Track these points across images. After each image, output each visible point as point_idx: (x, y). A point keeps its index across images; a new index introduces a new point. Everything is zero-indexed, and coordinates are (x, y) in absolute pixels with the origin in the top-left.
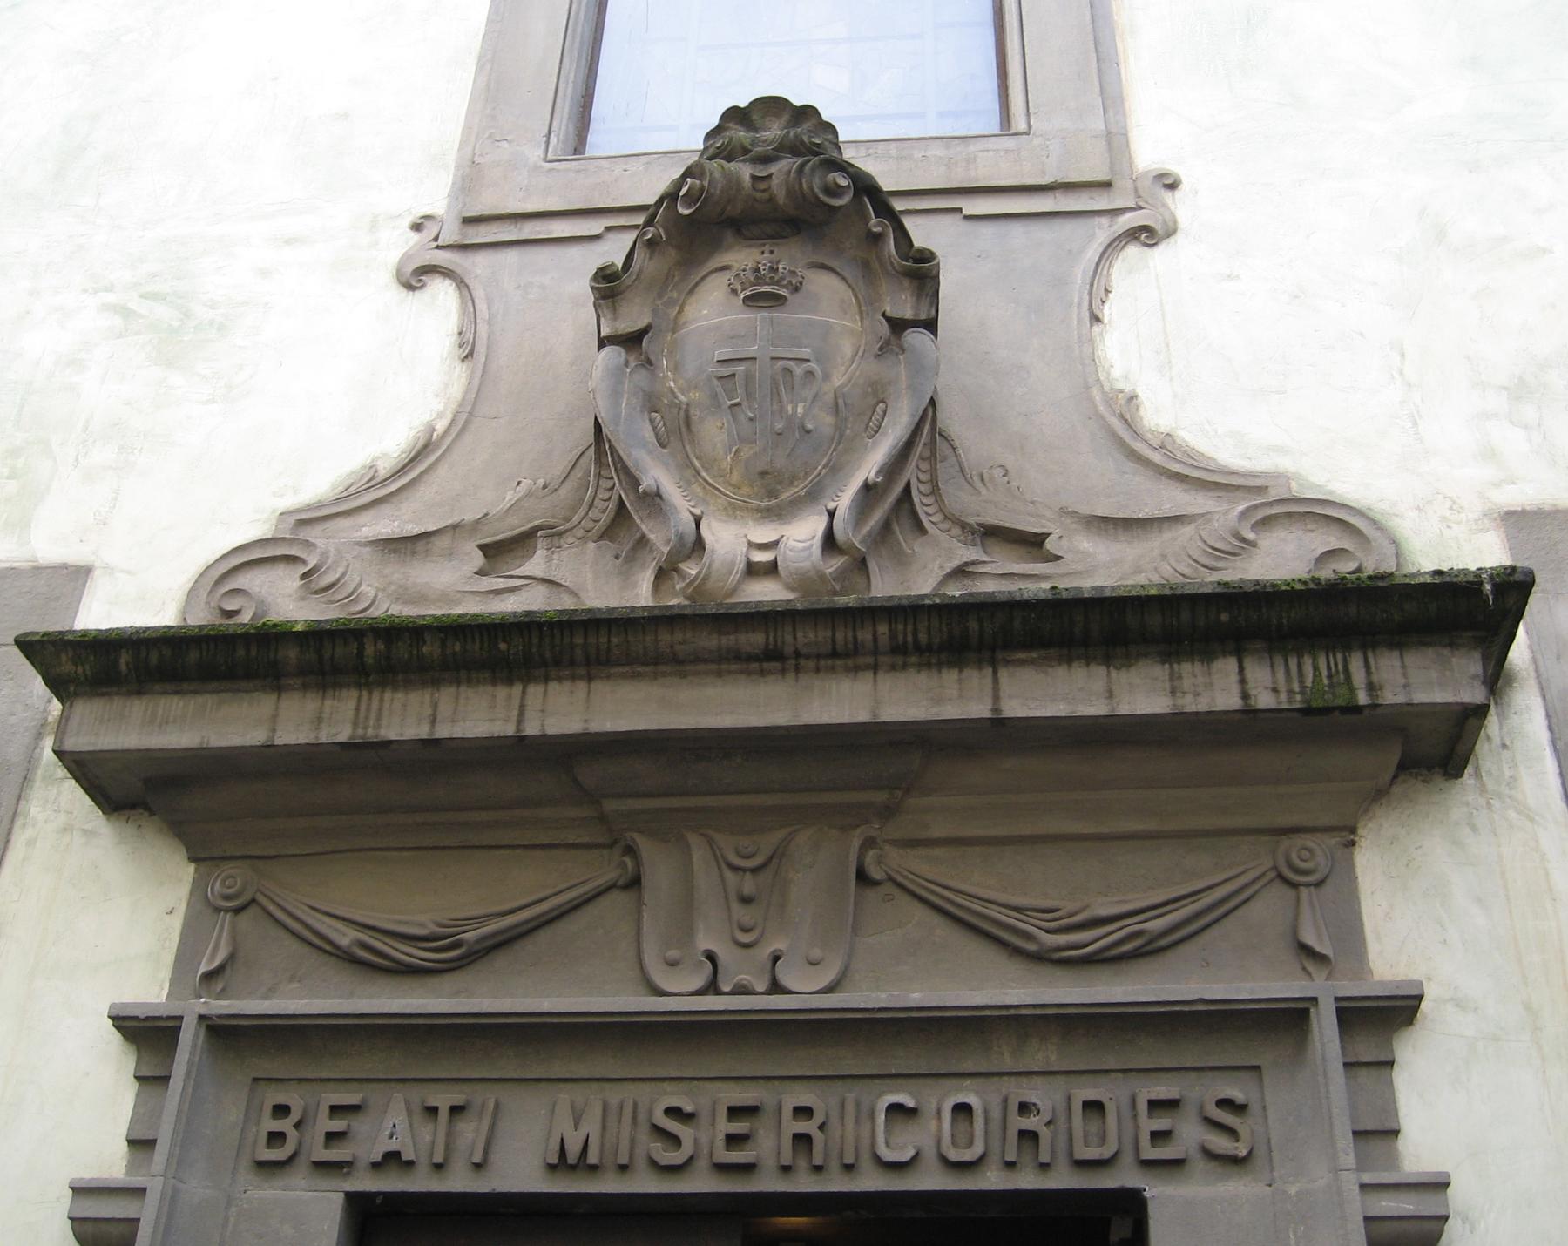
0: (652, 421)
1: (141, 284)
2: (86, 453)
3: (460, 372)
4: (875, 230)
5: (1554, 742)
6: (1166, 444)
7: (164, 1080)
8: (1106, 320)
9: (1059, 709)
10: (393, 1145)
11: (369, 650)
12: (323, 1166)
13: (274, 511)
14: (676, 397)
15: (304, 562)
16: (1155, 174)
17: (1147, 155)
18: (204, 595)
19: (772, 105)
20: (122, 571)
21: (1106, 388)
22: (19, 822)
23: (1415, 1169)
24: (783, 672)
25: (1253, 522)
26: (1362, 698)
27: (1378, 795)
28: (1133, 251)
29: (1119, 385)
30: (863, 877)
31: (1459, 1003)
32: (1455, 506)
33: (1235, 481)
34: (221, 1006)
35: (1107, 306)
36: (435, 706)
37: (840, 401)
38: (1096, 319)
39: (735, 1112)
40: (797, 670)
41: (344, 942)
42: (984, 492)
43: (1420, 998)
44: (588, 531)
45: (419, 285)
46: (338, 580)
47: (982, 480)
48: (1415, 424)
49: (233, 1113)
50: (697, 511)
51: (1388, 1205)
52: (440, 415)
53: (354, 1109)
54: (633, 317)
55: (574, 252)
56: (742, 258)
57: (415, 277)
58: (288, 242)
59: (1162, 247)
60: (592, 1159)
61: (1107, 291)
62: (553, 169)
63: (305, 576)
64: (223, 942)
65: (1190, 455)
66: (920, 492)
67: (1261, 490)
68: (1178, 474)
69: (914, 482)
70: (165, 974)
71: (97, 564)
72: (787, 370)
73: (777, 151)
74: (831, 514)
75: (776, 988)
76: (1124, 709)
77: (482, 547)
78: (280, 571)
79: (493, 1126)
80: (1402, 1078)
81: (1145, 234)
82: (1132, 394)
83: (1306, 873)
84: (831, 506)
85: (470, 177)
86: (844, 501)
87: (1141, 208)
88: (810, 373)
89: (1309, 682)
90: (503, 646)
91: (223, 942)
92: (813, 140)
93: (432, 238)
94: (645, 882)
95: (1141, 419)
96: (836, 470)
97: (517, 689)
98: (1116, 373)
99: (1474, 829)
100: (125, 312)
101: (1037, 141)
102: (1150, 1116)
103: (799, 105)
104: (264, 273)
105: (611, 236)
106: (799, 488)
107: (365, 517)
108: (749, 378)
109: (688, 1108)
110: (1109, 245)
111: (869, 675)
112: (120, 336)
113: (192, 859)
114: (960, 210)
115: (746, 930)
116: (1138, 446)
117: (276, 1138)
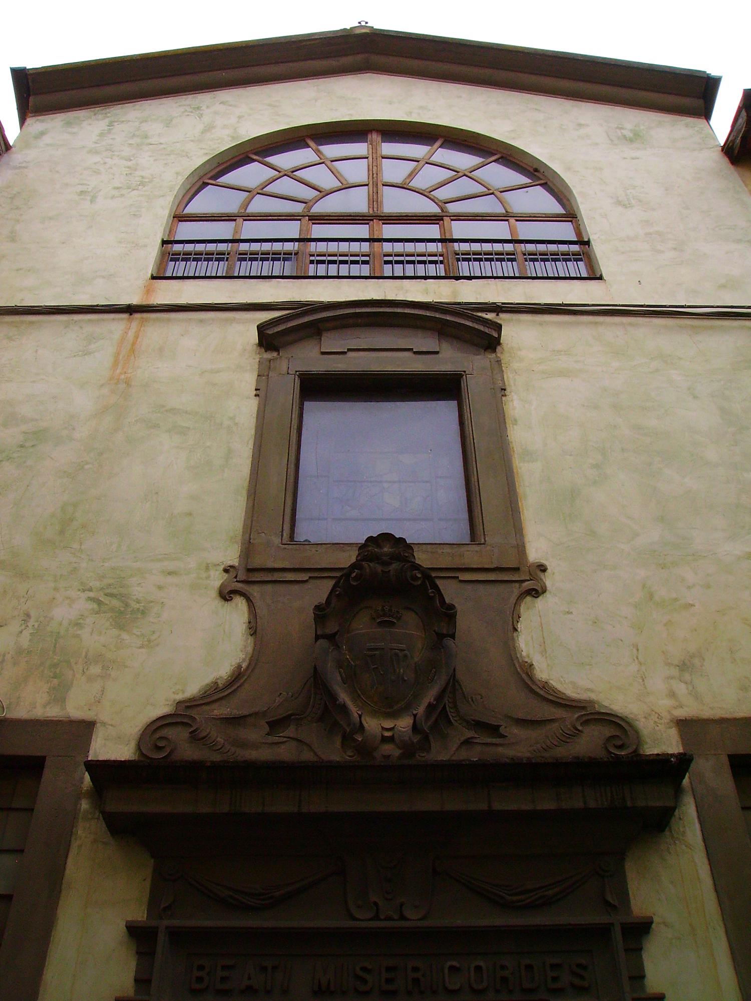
0: (340, 672)
1: (104, 589)
2: (87, 669)
3: (251, 640)
4: (430, 595)
5: (699, 817)
6: (545, 685)
7: (153, 953)
8: (519, 630)
9: (514, 807)
13: (174, 701)
14: (350, 663)
15: (191, 726)
17: (534, 554)
19: (387, 537)
20: (109, 725)
21: (520, 661)
25: (581, 721)
26: (629, 804)
28: (528, 599)
31: (666, 924)
32: (660, 717)
33: (574, 704)
35: (519, 624)
37: (417, 667)
38: (515, 630)
39: (389, 969)
42: (473, 706)
43: (652, 923)
44: (313, 718)
45: (230, 599)
47: (472, 700)
48: (643, 680)
50: (360, 713)
52: (244, 660)
54: (332, 627)
57: (226, 595)
58: (170, 573)
59: (541, 598)
62: (285, 548)
63: (191, 733)
65: (555, 691)
66: (450, 707)
67: (584, 708)
68: (551, 700)
70: (144, 908)
71: (97, 721)
72: (397, 655)
73: (391, 559)
75: (403, 918)
76: (539, 808)
77: (266, 722)
78: (179, 729)
81: (534, 592)
82: (531, 664)
84: (415, 712)
85: (248, 549)
86: (421, 710)
88: (405, 656)
92: (405, 554)
93: (234, 577)
95: (535, 675)
98: (524, 654)
99: (670, 853)
100: (99, 603)
101: (489, 548)
103: (398, 537)
104: (160, 588)
105: (312, 581)
107: (215, 706)
109: (369, 967)
110: (518, 598)
113: (153, 857)
114: (458, 577)
116: (534, 687)
117: (200, 979)
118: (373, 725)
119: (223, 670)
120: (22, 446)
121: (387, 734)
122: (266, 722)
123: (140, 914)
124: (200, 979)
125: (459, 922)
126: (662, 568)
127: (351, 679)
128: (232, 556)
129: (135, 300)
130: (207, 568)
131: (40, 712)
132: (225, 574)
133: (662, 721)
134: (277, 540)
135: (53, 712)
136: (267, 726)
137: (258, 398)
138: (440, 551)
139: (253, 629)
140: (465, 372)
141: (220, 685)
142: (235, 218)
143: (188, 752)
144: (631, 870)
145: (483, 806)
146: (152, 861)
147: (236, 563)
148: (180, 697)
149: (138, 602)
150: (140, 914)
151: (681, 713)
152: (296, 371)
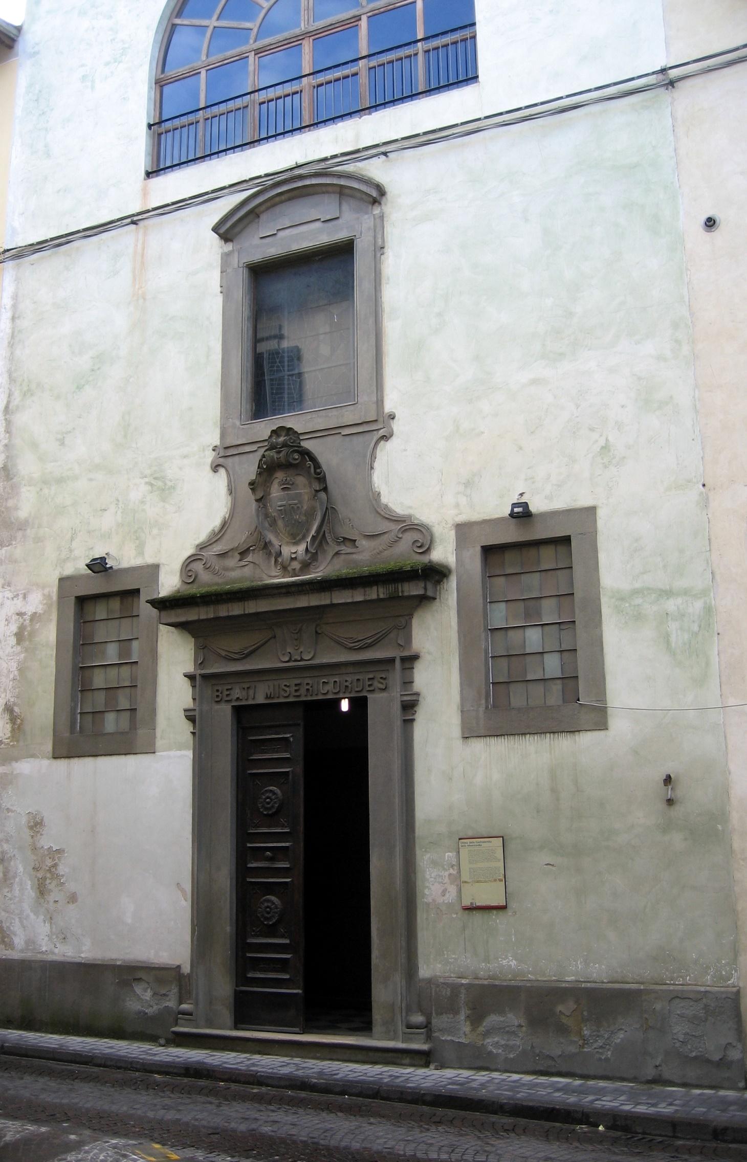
3: (230, 498)
7: (195, 686)
10: (238, 696)
11: (213, 598)
12: (226, 701)
16: (388, 415)
18: (184, 570)
21: (374, 491)
22: (159, 631)
23: (416, 690)
24: (292, 595)
28: (382, 442)
29: (377, 490)
30: (316, 632)
34: (203, 672)
36: (228, 608)
39: (296, 685)
40: (294, 595)
41: (223, 655)
46: (211, 566)
48: (442, 497)
49: (210, 692)
50: (280, 544)
51: (405, 698)
52: (227, 513)
53: (231, 689)
54: (260, 494)
55: (251, 455)
56: (280, 475)
57: (215, 468)
59: (389, 441)
60: (272, 696)
61: (375, 458)
64: (202, 657)
67: (404, 521)
69: (326, 530)
74: (307, 542)
77: (239, 553)
79: (255, 691)
80: (415, 671)
83: (400, 626)
86: (309, 540)
87: (384, 428)
88: (298, 507)
89: (390, 591)
90: (238, 595)
91: (202, 657)
94: (277, 636)
96: (308, 530)
97: (243, 603)
98: (376, 485)
101: (360, 406)
102: (369, 681)
104: (180, 469)
105: (260, 449)
106: (300, 537)
108: (285, 510)
109: (288, 685)
111: (308, 595)
112: (151, 493)
113: (193, 637)
115: (296, 646)
117: (218, 696)
119: (216, 523)
120: (93, 370)
121: (293, 556)
122: (239, 553)
123: (190, 668)
124: (218, 696)
126: (469, 403)
130: (204, 450)
132: (213, 452)
133: (448, 526)
134: (238, 423)
136: (239, 555)
137: (222, 294)
138: (330, 414)
140: (355, 236)
141: (216, 531)
142: (199, 71)
144: (415, 622)
145: (328, 602)
146: (193, 639)
148: (197, 542)
149: (171, 481)
152: (244, 263)
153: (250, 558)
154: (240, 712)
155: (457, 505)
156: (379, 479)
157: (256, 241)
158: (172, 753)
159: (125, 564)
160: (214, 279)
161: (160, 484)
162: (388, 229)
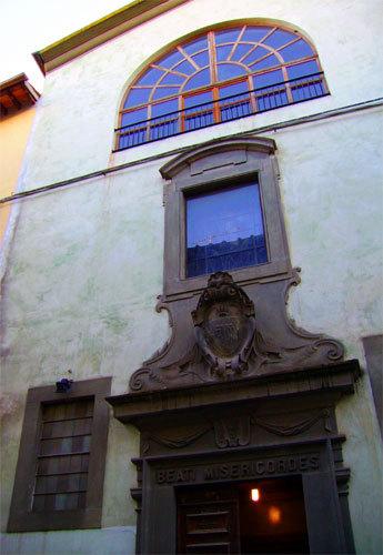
17: (294, 264)
27: (339, 400)
54: (200, 320)
56: (217, 306)
57: (159, 309)
85: (166, 287)
86: (242, 352)
96: (240, 346)
118: (222, 362)
119: (160, 346)
123: (137, 455)
125: (261, 445)
127: (211, 343)
128: (159, 290)
129: (106, 167)
131: (90, 377)
135: (96, 375)
139: (171, 324)
143: (151, 386)
144: (338, 413)
147: (161, 293)
150: (137, 455)
151: (364, 334)
153: (189, 369)
154: (179, 491)
155: (361, 325)
156: (292, 311)
157: (188, 177)
158: (116, 528)
159: (84, 378)
160: (159, 199)
161: (114, 322)
162: (281, 166)
